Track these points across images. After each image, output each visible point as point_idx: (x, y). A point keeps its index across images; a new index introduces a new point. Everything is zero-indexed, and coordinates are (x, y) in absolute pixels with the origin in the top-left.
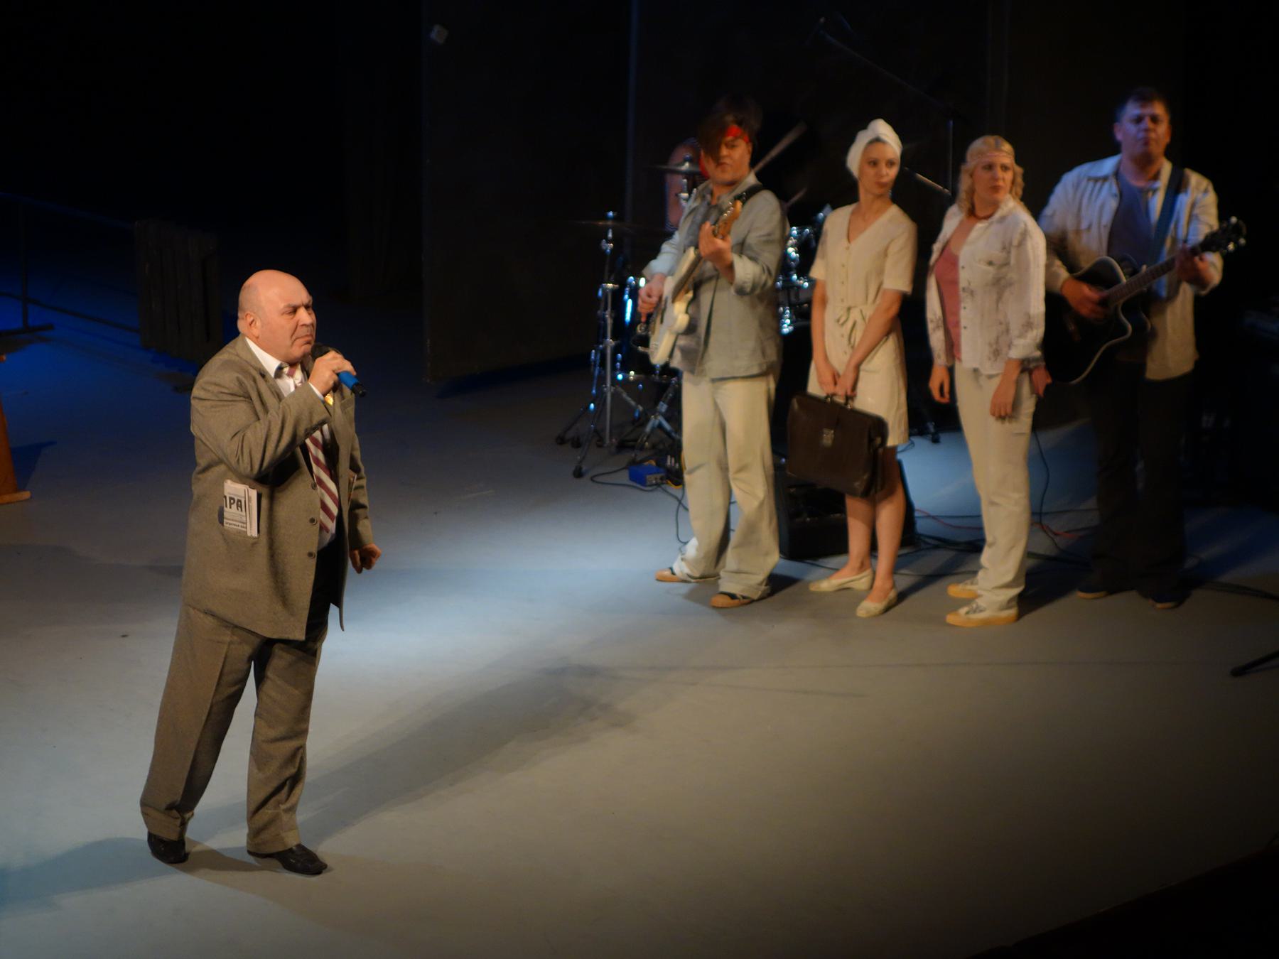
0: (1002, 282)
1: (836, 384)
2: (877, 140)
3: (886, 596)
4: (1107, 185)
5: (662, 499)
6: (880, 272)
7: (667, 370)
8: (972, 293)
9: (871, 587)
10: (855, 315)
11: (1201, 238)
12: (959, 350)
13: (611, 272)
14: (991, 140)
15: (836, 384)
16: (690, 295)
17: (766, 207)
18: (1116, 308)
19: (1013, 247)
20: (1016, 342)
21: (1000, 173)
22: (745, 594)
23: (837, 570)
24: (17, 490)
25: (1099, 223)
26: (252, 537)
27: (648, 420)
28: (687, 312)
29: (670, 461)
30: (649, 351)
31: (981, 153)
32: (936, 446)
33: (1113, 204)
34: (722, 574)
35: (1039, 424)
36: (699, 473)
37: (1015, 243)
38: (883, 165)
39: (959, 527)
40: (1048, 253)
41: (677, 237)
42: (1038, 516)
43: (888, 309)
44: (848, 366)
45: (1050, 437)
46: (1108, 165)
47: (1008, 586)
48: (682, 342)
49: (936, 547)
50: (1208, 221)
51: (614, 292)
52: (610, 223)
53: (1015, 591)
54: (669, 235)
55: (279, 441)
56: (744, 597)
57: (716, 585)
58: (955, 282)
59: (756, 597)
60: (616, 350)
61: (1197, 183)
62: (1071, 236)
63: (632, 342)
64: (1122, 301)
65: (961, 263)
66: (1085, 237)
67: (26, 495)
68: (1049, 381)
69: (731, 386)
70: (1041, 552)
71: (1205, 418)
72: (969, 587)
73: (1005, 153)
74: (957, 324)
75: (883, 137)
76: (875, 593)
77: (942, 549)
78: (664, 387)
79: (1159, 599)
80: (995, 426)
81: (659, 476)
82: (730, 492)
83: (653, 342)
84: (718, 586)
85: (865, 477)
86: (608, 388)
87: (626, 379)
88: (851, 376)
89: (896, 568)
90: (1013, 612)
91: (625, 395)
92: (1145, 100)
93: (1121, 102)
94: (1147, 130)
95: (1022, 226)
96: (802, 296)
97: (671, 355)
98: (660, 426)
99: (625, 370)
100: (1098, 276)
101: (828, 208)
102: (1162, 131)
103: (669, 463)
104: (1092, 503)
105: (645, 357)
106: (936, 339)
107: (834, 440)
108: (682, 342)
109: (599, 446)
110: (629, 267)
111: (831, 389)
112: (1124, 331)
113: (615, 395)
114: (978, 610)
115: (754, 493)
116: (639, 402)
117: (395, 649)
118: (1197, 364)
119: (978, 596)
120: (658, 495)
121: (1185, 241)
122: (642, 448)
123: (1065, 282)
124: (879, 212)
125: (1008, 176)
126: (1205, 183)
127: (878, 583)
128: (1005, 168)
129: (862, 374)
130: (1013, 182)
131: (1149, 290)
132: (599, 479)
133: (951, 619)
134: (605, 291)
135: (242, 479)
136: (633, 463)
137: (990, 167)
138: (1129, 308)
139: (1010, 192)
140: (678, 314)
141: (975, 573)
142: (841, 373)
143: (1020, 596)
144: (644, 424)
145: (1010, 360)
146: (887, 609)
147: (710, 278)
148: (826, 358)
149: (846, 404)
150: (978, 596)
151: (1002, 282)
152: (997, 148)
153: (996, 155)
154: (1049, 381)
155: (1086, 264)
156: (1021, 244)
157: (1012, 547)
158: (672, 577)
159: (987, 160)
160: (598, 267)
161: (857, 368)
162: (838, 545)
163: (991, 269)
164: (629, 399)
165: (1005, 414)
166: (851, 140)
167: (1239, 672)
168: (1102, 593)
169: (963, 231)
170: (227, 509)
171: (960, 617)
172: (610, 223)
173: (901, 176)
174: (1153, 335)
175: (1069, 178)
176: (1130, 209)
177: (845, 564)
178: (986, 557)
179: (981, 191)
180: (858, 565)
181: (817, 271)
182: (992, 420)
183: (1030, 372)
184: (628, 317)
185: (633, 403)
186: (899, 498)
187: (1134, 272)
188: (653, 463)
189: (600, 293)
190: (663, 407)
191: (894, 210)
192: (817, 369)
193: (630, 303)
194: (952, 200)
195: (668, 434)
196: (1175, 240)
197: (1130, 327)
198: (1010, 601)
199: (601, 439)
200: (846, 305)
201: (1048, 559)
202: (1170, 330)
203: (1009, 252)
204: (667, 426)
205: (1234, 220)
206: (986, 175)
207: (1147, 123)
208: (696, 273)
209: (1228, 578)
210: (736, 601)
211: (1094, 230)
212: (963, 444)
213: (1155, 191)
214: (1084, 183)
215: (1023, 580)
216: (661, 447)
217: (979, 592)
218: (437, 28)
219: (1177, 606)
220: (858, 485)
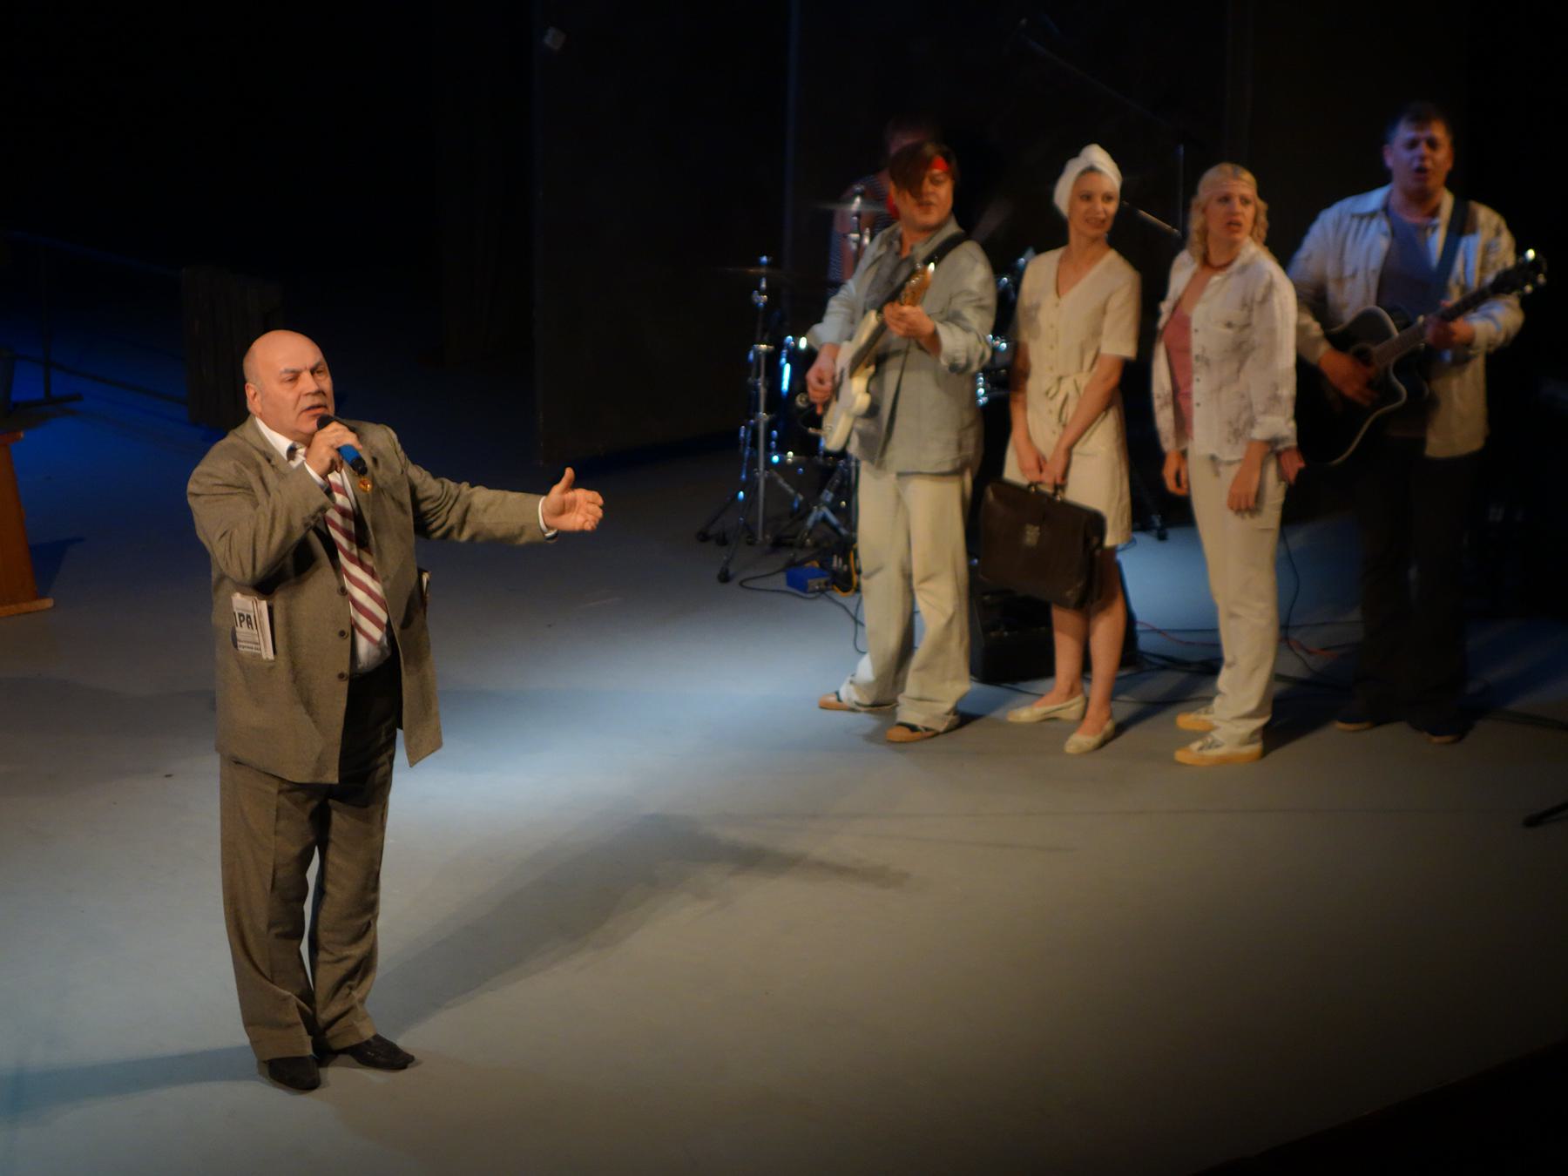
1: (1041, 470)
2: (1091, 170)
3: (1101, 727)
4: (1375, 223)
5: (826, 610)
6: (1096, 333)
8: (1207, 363)
10: (1068, 386)
12: (1191, 427)
13: (764, 331)
14: (1227, 168)
15: (1041, 470)
16: (872, 369)
18: (1386, 370)
19: (1256, 304)
20: (1260, 419)
21: (1239, 207)
22: (928, 725)
23: (1041, 696)
24: (40, 596)
25: (1366, 268)
26: (268, 661)
27: (810, 512)
28: (868, 391)
29: (837, 563)
30: (822, 433)
32: (1161, 544)
33: (1383, 244)
34: (901, 699)
35: (1291, 515)
36: (878, 577)
37: (1258, 297)
38: (1099, 199)
39: (1188, 643)
40: (1300, 309)
42: (1287, 631)
43: (1106, 379)
44: (1058, 445)
45: (1298, 538)
46: (1375, 199)
47: (1251, 716)
48: (860, 425)
49: (1164, 668)
50: (1505, 256)
52: (763, 270)
53: (1259, 723)
54: (837, 286)
55: (271, 536)
57: (893, 713)
58: (1186, 350)
59: (941, 728)
60: (770, 426)
61: (1486, 217)
62: (1332, 288)
63: (799, 423)
64: (1392, 361)
65: (1194, 324)
66: (1348, 286)
67: (48, 603)
68: (1302, 465)
70: (1291, 674)
72: (1203, 717)
73: (1244, 184)
74: (1188, 396)
75: (1099, 166)
76: (1088, 723)
77: (1171, 671)
78: (835, 477)
79: (1435, 732)
80: (1234, 522)
81: (823, 580)
82: (913, 603)
83: (826, 423)
85: (1079, 585)
86: (761, 473)
87: (782, 461)
88: (1061, 460)
89: (1113, 694)
90: (1256, 748)
92: (1421, 120)
93: (1391, 122)
94: (1423, 158)
95: (1267, 277)
97: (848, 441)
98: (825, 520)
99: (782, 452)
100: (1350, 339)
101: (1030, 252)
102: (1442, 157)
103: (835, 565)
104: (1355, 615)
105: (816, 440)
106: (1164, 419)
108: (860, 425)
109: (750, 544)
111: (1035, 476)
112: (1397, 396)
113: (770, 482)
114: (1215, 745)
115: (940, 605)
116: (798, 490)
117: (459, 803)
118: (1489, 440)
119: (1213, 728)
120: (822, 603)
122: (802, 546)
123: (1288, 450)
124: (1094, 260)
125: (1249, 212)
127: (1092, 711)
128: (1245, 201)
129: (1075, 458)
130: (1255, 221)
132: (750, 584)
133: (1180, 756)
134: (757, 353)
135: (241, 588)
136: (792, 564)
137: (1226, 199)
138: (1402, 368)
139: (1251, 234)
140: (857, 392)
141: (1210, 700)
142: (1048, 457)
143: (1265, 727)
145: (1252, 442)
146: (1104, 743)
147: (897, 353)
148: (1029, 439)
149: (1055, 494)
150: (1213, 728)
153: (1235, 188)
154: (1302, 465)
155: (1348, 315)
157: (1254, 670)
158: (839, 706)
160: (749, 325)
161: (1069, 452)
162: (1045, 668)
163: (1230, 332)
164: (786, 486)
165: (1246, 505)
167: (1533, 822)
168: (1366, 725)
169: (1196, 286)
170: (238, 629)
171: (1191, 753)
172: (763, 270)
173: (1121, 215)
175: (1328, 219)
176: (1406, 242)
178: (1224, 679)
179: (1215, 228)
180: (1066, 690)
182: (1230, 514)
183: (1278, 455)
184: (785, 386)
185: (791, 491)
186: (1117, 610)
188: (817, 565)
189: (751, 356)
190: (828, 496)
191: (1112, 255)
193: (787, 369)
194: (1179, 244)
195: (835, 529)
197: (1403, 389)
198: (1254, 733)
200: (1056, 374)
202: (1456, 399)
203: (1251, 310)
204: (833, 519)
205: (1531, 254)
206: (1218, 210)
207: (1423, 149)
208: (880, 344)
209: (1518, 705)
210: (916, 735)
212: (1196, 542)
213: (1435, 228)
214: (1346, 222)
215: (1269, 709)
216: (826, 544)
217: (1216, 723)
218: (552, 32)
219: (1454, 742)
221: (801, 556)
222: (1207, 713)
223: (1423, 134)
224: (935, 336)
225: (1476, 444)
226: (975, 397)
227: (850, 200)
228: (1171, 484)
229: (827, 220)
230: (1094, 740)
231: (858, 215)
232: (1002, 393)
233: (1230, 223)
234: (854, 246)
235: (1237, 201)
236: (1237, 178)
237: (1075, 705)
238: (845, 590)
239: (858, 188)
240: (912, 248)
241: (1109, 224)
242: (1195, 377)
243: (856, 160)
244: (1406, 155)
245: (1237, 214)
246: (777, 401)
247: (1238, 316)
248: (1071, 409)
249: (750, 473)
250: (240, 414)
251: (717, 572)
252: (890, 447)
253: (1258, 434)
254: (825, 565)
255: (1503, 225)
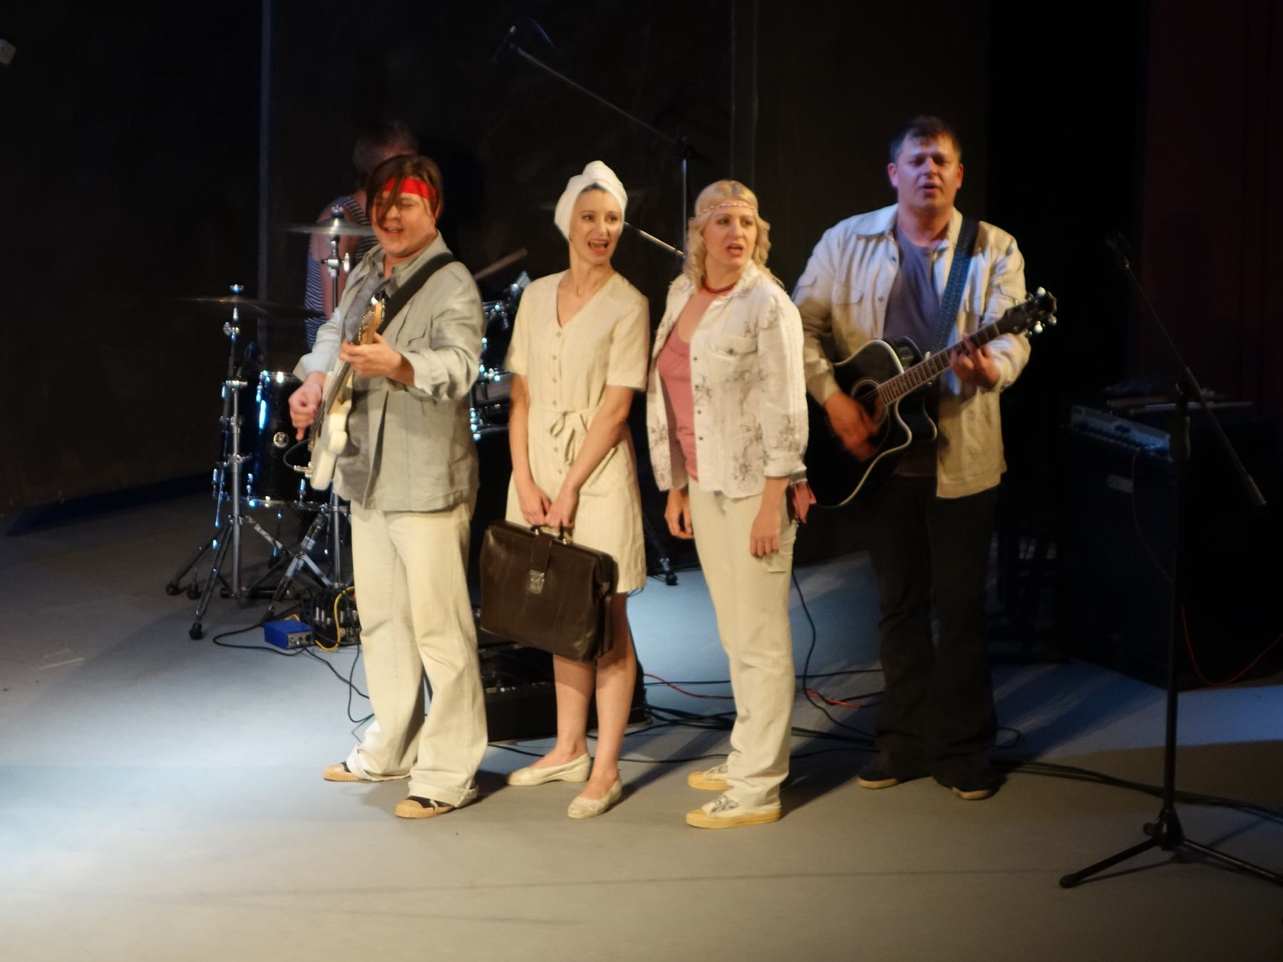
0: (747, 376)
1: (545, 513)
2: (595, 187)
3: (608, 789)
4: (882, 246)
7: (326, 495)
8: (708, 392)
9: (588, 779)
10: (574, 422)
11: (1000, 315)
13: (237, 364)
14: (726, 185)
15: (545, 513)
16: (348, 404)
17: (455, 292)
18: (892, 407)
21: (740, 230)
27: (290, 561)
31: (714, 204)
33: (891, 270)
36: (381, 632)
38: (602, 219)
41: (337, 316)
42: (805, 684)
43: (614, 412)
44: (565, 485)
45: (819, 582)
46: (883, 218)
47: (766, 773)
48: (343, 461)
49: (674, 723)
50: (1015, 291)
51: (241, 391)
52: (234, 300)
53: (778, 780)
54: (322, 317)
56: (440, 804)
58: (686, 379)
60: (245, 468)
61: (997, 239)
62: (837, 313)
63: (280, 463)
64: (898, 400)
65: (693, 352)
66: (854, 311)
68: (813, 501)
69: (407, 519)
70: (810, 728)
71: (1023, 547)
72: (716, 776)
73: (745, 202)
75: (602, 184)
76: (593, 784)
77: (687, 726)
81: (304, 635)
84: (408, 790)
85: (589, 635)
88: (568, 502)
89: (621, 752)
90: (775, 807)
91: (258, 528)
92: (927, 134)
94: (929, 175)
96: (493, 394)
98: (306, 568)
99: (259, 494)
101: (524, 277)
102: (952, 174)
106: (660, 455)
107: (545, 585)
109: (224, 596)
110: (262, 358)
111: (540, 519)
113: (246, 528)
115: (451, 656)
116: (276, 537)
120: (304, 660)
121: (982, 319)
122: (282, 598)
124: (602, 282)
125: (751, 233)
126: (1008, 240)
127: (597, 772)
128: (746, 222)
129: (582, 498)
130: (757, 242)
131: (937, 382)
133: (692, 818)
134: (229, 389)
136: (270, 618)
138: (911, 405)
139: (753, 258)
140: (336, 423)
142: (553, 499)
143: (783, 785)
144: (284, 567)
149: (561, 537)
151: (747, 376)
152: (736, 196)
153: (732, 207)
154: (813, 501)
156: (773, 325)
159: (721, 212)
160: (218, 358)
161: (577, 491)
162: (549, 730)
163: (732, 359)
164: (263, 533)
166: (562, 188)
167: (1070, 881)
168: (893, 781)
169: (695, 312)
171: (703, 816)
173: (628, 237)
174: (943, 442)
175: (834, 236)
177: (552, 747)
179: (715, 251)
180: (570, 749)
181: (517, 361)
185: (269, 539)
187: (917, 359)
190: (309, 543)
191: (618, 281)
192: (519, 491)
195: (317, 578)
196: (970, 316)
197: (910, 433)
198: (770, 792)
199: (227, 587)
201: (820, 735)
202: (966, 434)
203: (756, 336)
206: (720, 232)
207: (930, 165)
209: (1054, 755)
211: (867, 304)
213: (941, 252)
215: (786, 765)
216: (307, 596)
217: (730, 782)
220: (580, 645)
221: (280, 608)
222: (720, 771)
223: (930, 150)
224: (405, 365)
225: (992, 481)
226: (471, 433)
227: (328, 223)
228: (674, 529)
229: (305, 241)
230: (601, 803)
231: (337, 239)
232: (497, 429)
233: (729, 248)
234: (333, 273)
235: (737, 222)
236: (736, 196)
237: (581, 763)
238: (329, 645)
239: (337, 210)
240: (393, 270)
241: (612, 247)
242: (696, 408)
243: (338, 176)
244: (912, 172)
245: (736, 238)
246: (253, 440)
247: (742, 343)
248: (577, 445)
249: (224, 521)
250: (768, 265)
251: (190, 627)
252: (378, 484)
253: (774, 469)
254: (306, 618)
255: (1015, 246)
